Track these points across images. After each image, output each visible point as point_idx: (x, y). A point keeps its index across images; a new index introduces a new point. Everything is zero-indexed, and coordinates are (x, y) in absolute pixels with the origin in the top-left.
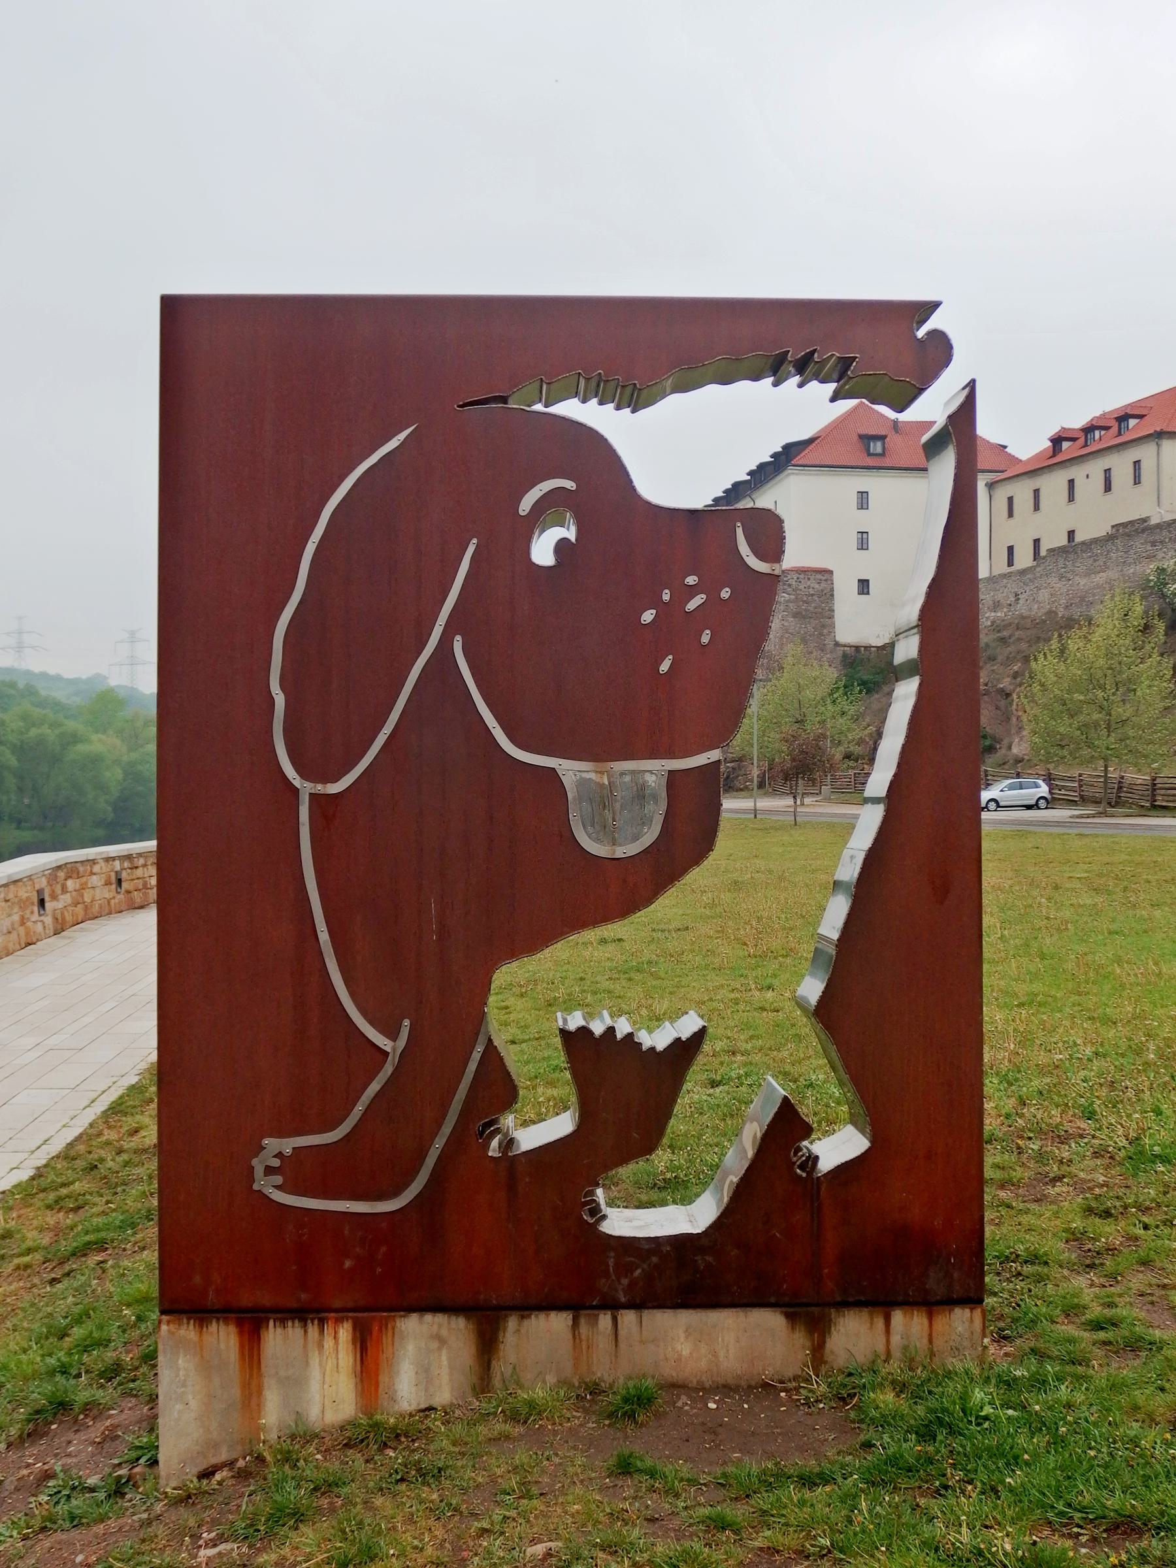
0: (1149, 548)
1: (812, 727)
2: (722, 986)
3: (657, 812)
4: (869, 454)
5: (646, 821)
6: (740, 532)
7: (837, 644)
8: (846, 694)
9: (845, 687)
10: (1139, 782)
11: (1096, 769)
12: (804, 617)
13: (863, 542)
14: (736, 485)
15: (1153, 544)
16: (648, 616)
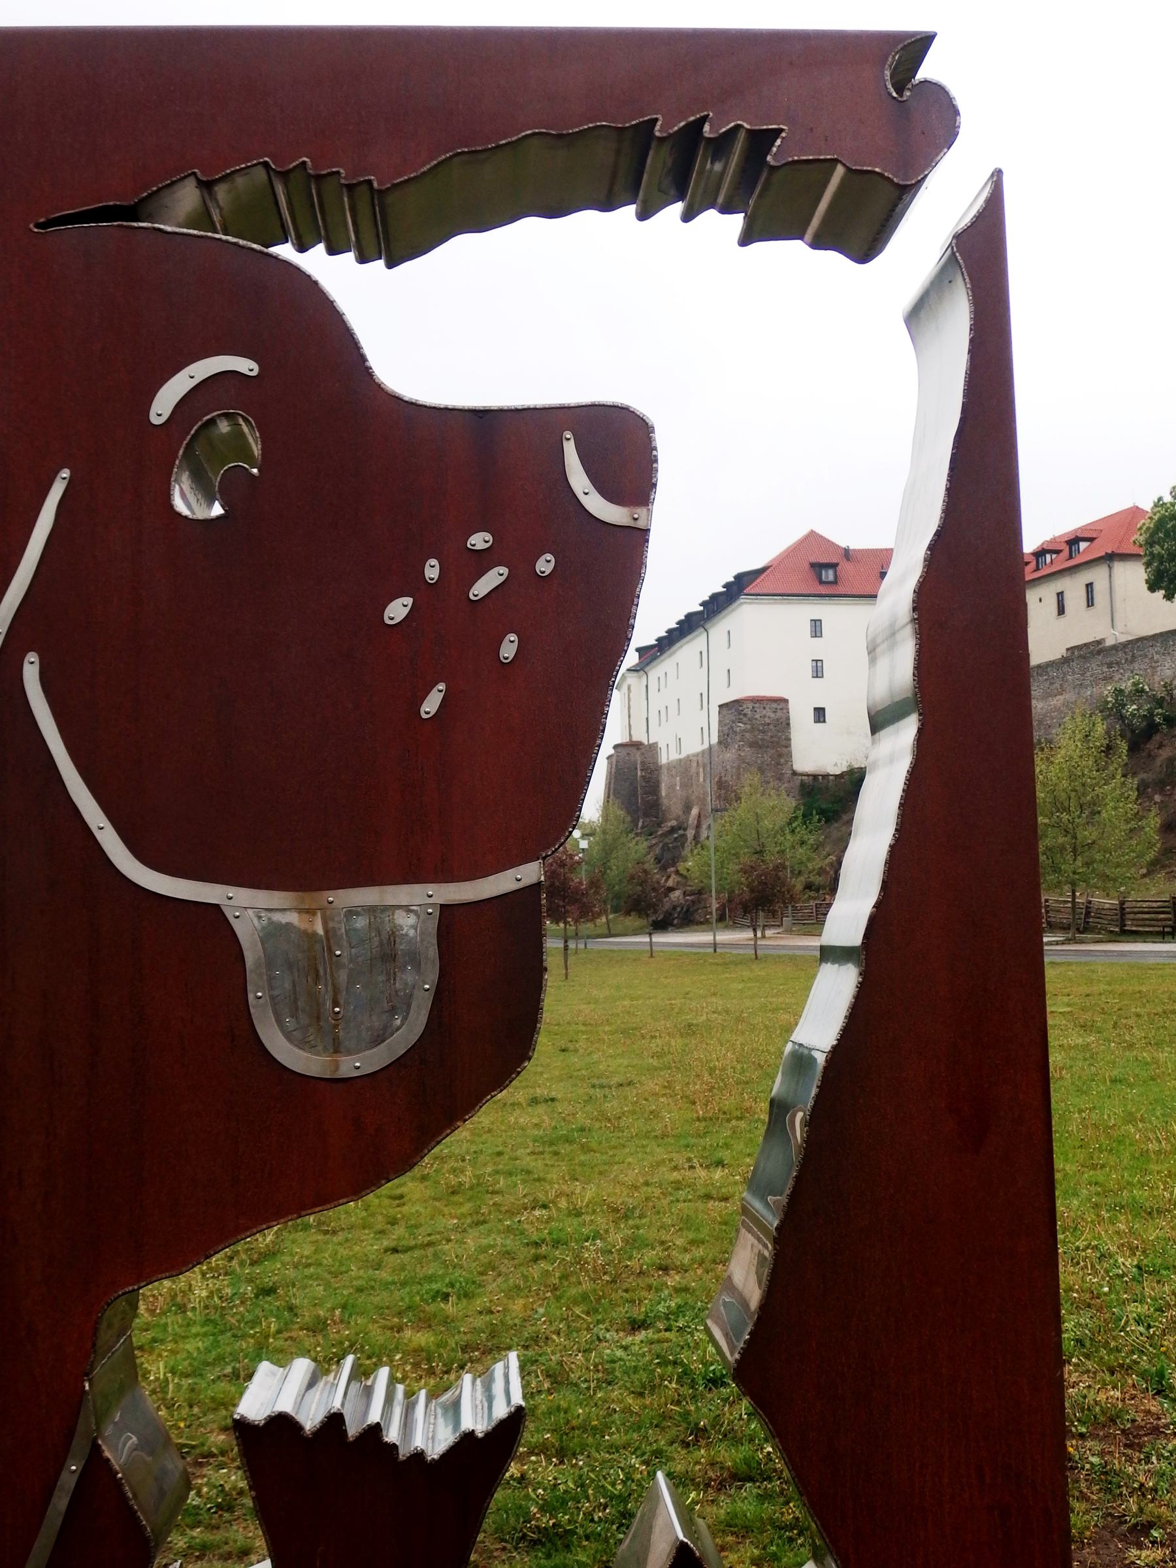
0: (1105, 669)
1: (771, 858)
2: (663, 1161)
3: (422, 984)
4: (821, 582)
5: (400, 1004)
6: (570, 450)
7: (794, 773)
8: (805, 823)
9: (804, 816)
10: (1107, 906)
11: (1061, 895)
12: (760, 747)
13: (818, 670)
14: (689, 616)
15: (1110, 665)
16: (398, 610)
